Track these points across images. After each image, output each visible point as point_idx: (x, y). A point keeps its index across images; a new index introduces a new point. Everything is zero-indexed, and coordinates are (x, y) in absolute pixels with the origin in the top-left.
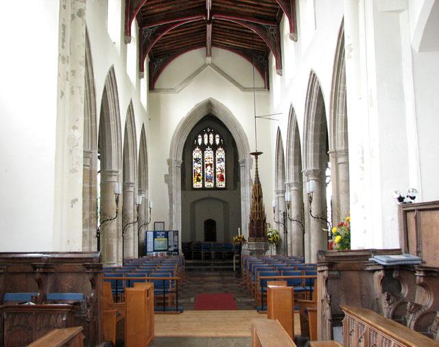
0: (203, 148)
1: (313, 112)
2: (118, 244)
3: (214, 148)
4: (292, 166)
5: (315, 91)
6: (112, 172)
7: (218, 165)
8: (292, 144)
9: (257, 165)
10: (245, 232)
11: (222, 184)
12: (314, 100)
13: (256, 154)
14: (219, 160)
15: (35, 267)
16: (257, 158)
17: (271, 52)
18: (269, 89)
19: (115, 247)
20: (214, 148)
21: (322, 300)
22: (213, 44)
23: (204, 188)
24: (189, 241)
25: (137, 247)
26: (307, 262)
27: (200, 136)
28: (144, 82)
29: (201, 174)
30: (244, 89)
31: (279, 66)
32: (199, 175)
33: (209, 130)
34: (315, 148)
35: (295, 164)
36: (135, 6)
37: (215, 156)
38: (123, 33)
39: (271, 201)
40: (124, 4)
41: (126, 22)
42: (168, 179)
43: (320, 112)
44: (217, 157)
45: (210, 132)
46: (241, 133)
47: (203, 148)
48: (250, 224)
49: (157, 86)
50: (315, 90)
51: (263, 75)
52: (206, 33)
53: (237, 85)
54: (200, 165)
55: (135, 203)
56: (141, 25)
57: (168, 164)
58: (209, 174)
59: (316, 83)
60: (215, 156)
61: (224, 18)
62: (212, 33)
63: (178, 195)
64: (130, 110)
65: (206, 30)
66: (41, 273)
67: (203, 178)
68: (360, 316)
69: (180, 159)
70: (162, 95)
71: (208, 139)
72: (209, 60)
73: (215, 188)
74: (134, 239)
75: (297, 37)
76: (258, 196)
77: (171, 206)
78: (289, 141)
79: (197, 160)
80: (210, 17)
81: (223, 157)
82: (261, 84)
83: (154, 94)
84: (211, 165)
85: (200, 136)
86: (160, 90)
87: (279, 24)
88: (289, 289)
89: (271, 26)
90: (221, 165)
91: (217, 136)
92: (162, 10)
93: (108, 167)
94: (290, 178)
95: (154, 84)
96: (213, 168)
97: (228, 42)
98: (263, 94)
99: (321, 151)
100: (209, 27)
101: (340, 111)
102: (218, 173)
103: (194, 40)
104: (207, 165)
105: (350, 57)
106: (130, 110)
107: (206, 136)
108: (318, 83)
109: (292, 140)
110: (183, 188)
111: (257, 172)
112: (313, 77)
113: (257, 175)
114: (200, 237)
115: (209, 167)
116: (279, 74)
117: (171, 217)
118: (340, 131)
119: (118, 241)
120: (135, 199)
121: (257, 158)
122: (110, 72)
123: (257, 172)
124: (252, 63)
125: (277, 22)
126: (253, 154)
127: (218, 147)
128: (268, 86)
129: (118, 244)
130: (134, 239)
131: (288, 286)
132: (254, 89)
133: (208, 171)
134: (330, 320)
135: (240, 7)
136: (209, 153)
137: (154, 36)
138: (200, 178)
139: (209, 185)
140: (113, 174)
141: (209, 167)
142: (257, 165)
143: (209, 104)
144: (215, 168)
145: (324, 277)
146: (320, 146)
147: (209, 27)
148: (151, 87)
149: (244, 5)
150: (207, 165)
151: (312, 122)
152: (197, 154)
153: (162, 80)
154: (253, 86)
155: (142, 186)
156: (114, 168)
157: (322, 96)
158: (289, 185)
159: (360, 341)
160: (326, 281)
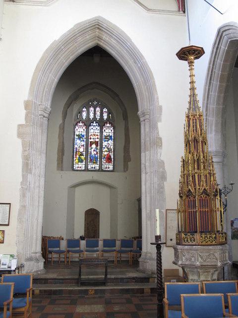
0: (88, 124)
3: (102, 124)
7: (105, 144)
32: (82, 155)
33: (95, 103)
44: (105, 134)
47: (88, 124)
60: (101, 132)
67: (86, 158)
79: (80, 137)
84: (96, 143)
104: (92, 143)
107: (92, 109)
115: (94, 146)
136: (94, 130)
141: (94, 146)
150: (92, 143)
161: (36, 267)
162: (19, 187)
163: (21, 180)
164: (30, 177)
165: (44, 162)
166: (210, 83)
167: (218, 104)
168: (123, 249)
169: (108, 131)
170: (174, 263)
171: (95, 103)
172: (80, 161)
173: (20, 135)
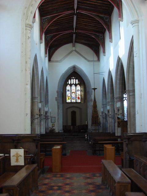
0: (71, 85)
1: (119, 73)
2: (38, 128)
3: (76, 85)
4: (109, 94)
5: (120, 64)
6: (35, 97)
7: (77, 93)
8: (110, 85)
9: (95, 94)
10: (90, 122)
11: (79, 101)
12: (119, 68)
13: (95, 89)
14: (77, 90)
15: (14, 140)
16: (94, 91)
17: (101, 45)
18: (99, 61)
19: (37, 129)
20: (76, 85)
21: (126, 152)
22: (76, 42)
23: (71, 103)
24: (65, 125)
25: (45, 128)
26: (116, 135)
27: (69, 80)
28: (47, 59)
29: (70, 96)
30: (89, 61)
31: (104, 52)
32: (69, 97)
33: (73, 78)
34: (120, 87)
35: (111, 94)
36: (44, 27)
37: (76, 89)
38: (40, 39)
39: (100, 109)
40: (40, 27)
41: (40, 34)
42: (56, 99)
43: (122, 71)
44: (77, 89)
45: (74, 78)
46: (88, 79)
47: (71, 85)
48: (92, 119)
49: (52, 59)
50: (120, 64)
51: (97, 56)
52: (73, 37)
53: (86, 59)
54: (70, 93)
55: (38, 108)
56: (46, 34)
57: (57, 93)
58: (73, 96)
59: (120, 61)
60: (76, 89)
61: (80, 31)
62: (76, 37)
63: (61, 106)
64: (42, 71)
65: (73, 36)
66: (16, 143)
67: (71, 98)
68: (141, 159)
69: (62, 90)
70: (54, 64)
71: (73, 81)
72: (74, 48)
73: (76, 103)
74: (43, 125)
75: (112, 41)
76: (95, 106)
77: (58, 111)
78: (108, 84)
79: (68, 90)
80: (75, 32)
81: (80, 89)
82: (96, 58)
83: (51, 63)
84: (74, 92)
85: (69, 80)
86: (53, 61)
87: (104, 34)
88: (112, 148)
89: (101, 35)
90: (79, 93)
91: (77, 80)
92: (55, 28)
93: (34, 96)
94: (109, 99)
95: (51, 59)
96: (75, 94)
97: (82, 41)
98: (96, 63)
99: (122, 89)
100: (74, 35)
101: (131, 74)
102: (77, 96)
103: (67, 40)
104: (73, 93)
105: (136, 56)
106: (42, 71)
107: (72, 80)
108: (121, 61)
109: (110, 83)
110: (63, 103)
111: (95, 96)
112: (119, 60)
113: (95, 98)
114: (70, 123)
115: (73, 93)
116: (104, 55)
117: (58, 115)
118: (131, 82)
119: (38, 126)
120: (38, 105)
121: (94, 91)
122: (35, 57)
123: (95, 96)
124: (92, 50)
125: (103, 33)
126: (93, 89)
127: (77, 85)
128: (99, 60)
129: (38, 128)
130: (43, 125)
131: (112, 146)
132: (93, 61)
133: (73, 95)
134: (129, 160)
135: (87, 27)
136: (73, 87)
137: (51, 39)
138: (70, 98)
139: (74, 101)
140: (36, 98)
141: (73, 93)
142: (95, 94)
143: (74, 67)
144: (76, 94)
145: (126, 143)
146: (122, 87)
147: (74, 35)
148: (49, 60)
149: (89, 26)
150: (73, 93)
151: (118, 77)
152: (68, 88)
153: (54, 57)
154: (93, 60)
155: (47, 102)
156: (36, 96)
157: (135, 91)
158: (109, 102)
159: (140, 168)
160: (127, 145)
161: (45, 133)
162: (57, 113)
163: (57, 111)
164: (59, 111)
165: (62, 106)
166: (130, 57)
167: (119, 89)
168: (72, 16)
169: (79, 88)
170: (54, 124)
171: (73, 78)
172: (69, 99)
173: (56, 100)
